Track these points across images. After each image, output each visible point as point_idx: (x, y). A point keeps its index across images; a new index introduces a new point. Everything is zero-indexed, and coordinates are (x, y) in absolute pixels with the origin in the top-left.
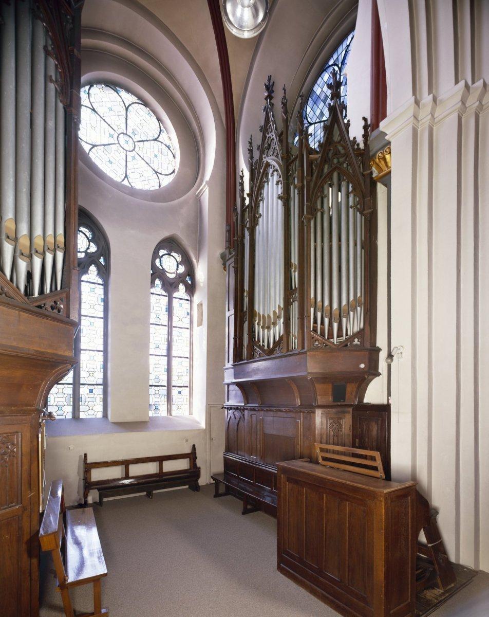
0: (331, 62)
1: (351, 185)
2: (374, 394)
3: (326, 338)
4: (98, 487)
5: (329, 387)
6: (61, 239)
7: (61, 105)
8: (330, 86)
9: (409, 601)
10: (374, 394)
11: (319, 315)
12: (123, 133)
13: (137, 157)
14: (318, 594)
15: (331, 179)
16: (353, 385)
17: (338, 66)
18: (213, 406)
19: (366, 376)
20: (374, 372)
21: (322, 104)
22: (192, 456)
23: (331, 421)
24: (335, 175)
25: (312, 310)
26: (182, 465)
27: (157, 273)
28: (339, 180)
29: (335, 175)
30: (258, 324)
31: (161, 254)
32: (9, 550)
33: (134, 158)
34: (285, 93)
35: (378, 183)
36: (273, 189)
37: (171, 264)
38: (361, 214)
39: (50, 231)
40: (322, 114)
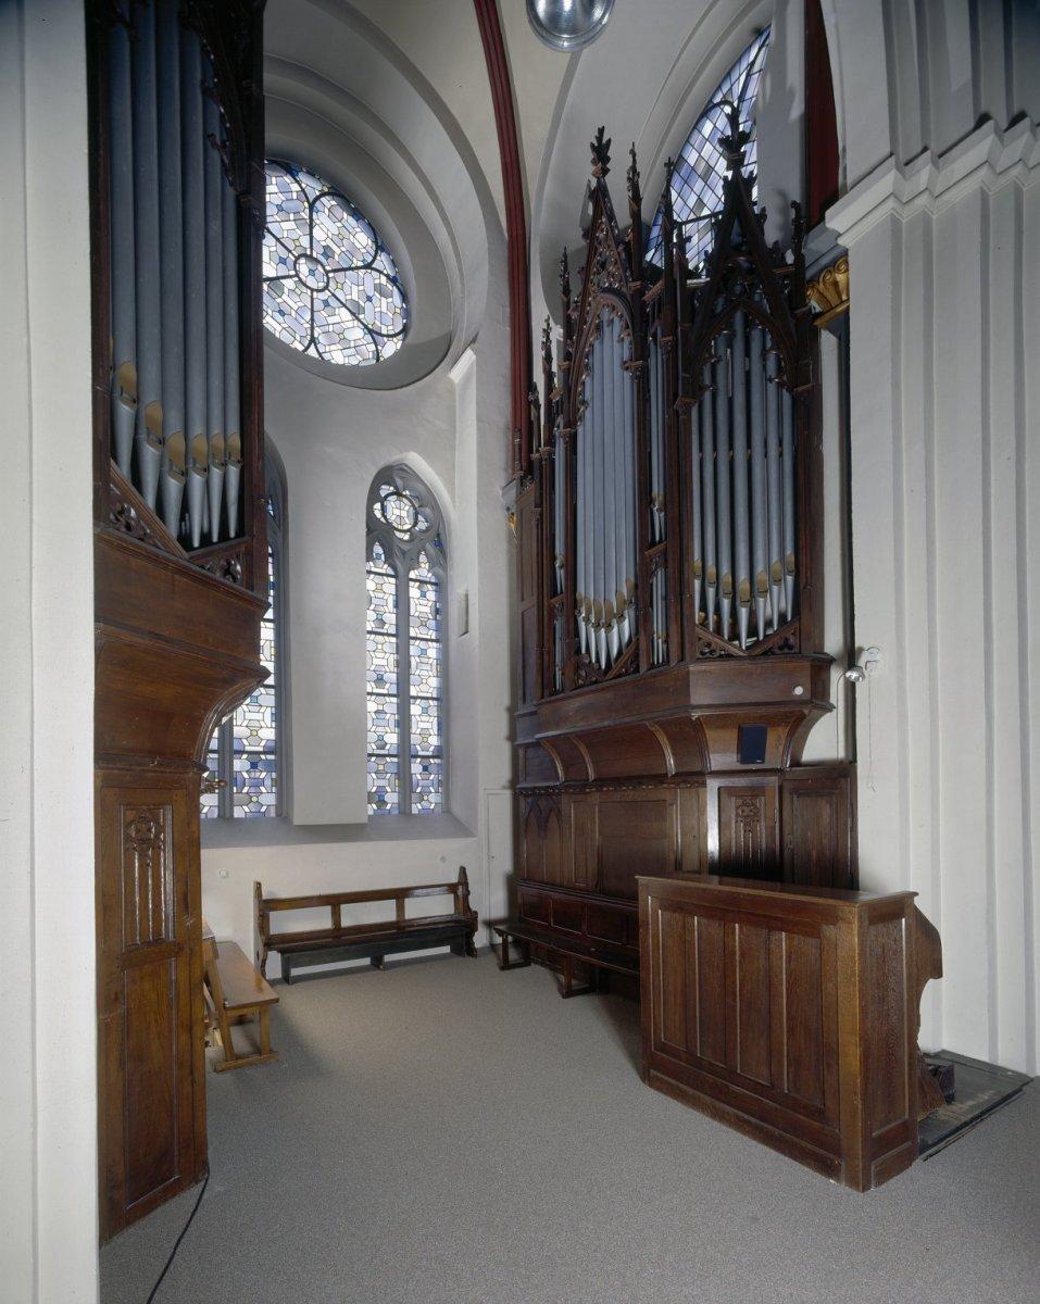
0: (717, 99)
1: (769, 337)
2: (822, 742)
3: (726, 637)
4: (281, 946)
5: (731, 736)
6: (235, 441)
7: (231, 192)
8: (724, 142)
9: (907, 1116)
10: (822, 742)
11: (711, 592)
12: (305, 255)
13: (333, 302)
14: (727, 1117)
15: (730, 325)
16: (780, 729)
17: (731, 104)
18: (492, 792)
19: (806, 712)
20: (818, 700)
21: (699, 185)
22: (459, 889)
23: (740, 801)
24: (738, 317)
25: (697, 583)
26: (438, 907)
27: (378, 532)
28: (748, 325)
29: (738, 317)
30: (587, 620)
31: (383, 493)
32: (156, 1021)
33: (326, 303)
34: (634, 161)
35: (823, 331)
36: (611, 349)
37: (404, 514)
38: (790, 391)
39: (216, 430)
40: (700, 203)
